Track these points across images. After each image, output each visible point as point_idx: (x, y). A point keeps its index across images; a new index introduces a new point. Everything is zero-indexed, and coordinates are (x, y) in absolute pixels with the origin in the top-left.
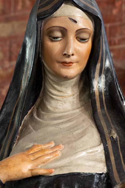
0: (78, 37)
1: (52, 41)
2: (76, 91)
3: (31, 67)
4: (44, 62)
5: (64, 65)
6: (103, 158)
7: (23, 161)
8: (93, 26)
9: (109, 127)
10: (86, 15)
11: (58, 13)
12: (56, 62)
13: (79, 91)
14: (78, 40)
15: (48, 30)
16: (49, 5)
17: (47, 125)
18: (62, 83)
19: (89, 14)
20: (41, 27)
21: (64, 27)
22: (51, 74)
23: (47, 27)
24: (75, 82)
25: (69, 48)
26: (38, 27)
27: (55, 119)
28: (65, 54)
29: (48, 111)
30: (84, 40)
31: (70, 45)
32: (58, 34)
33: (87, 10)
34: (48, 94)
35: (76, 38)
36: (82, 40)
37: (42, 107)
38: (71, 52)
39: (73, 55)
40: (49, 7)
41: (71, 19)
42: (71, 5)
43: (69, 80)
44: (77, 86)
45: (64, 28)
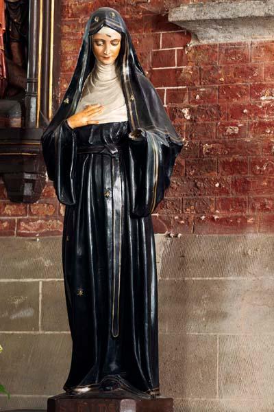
6: (126, 112)
7: (83, 117)
9: (130, 93)
11: (100, 32)
17: (97, 91)
27: (102, 86)
29: (98, 79)
32: (101, 43)
37: (95, 76)
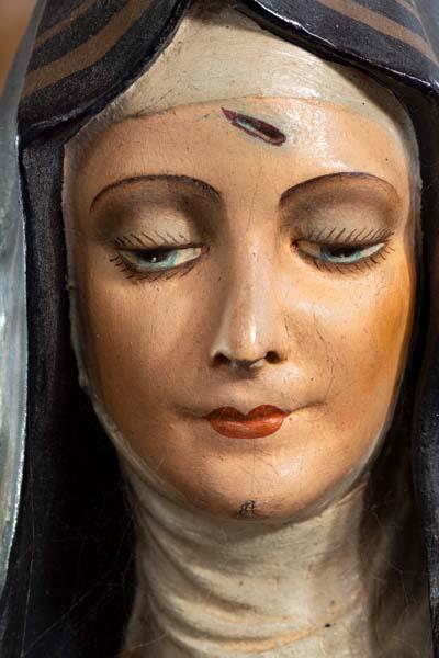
0: (303, 239)
1: (134, 275)
2: (348, 595)
3: (17, 463)
4: (104, 418)
5: (222, 431)
8: (411, 151)
10: (350, 80)
11: (155, 84)
12: (174, 417)
13: (365, 599)
14: (307, 257)
15: (99, 206)
16: (94, 39)
18: (244, 549)
19: (366, 73)
20: (57, 191)
21: (205, 180)
22: (162, 496)
23: (93, 185)
24: (332, 535)
25: (239, 318)
26: (33, 190)
28: (221, 359)
30: (350, 249)
31: (249, 295)
32: (168, 227)
33: (348, 45)
34: (162, 632)
35: (295, 243)
36: (336, 253)
38: (253, 343)
39: (273, 357)
40: (94, 50)
41: (237, 119)
42: (238, 25)
43: (289, 529)
44: (353, 561)
45: (203, 185)
